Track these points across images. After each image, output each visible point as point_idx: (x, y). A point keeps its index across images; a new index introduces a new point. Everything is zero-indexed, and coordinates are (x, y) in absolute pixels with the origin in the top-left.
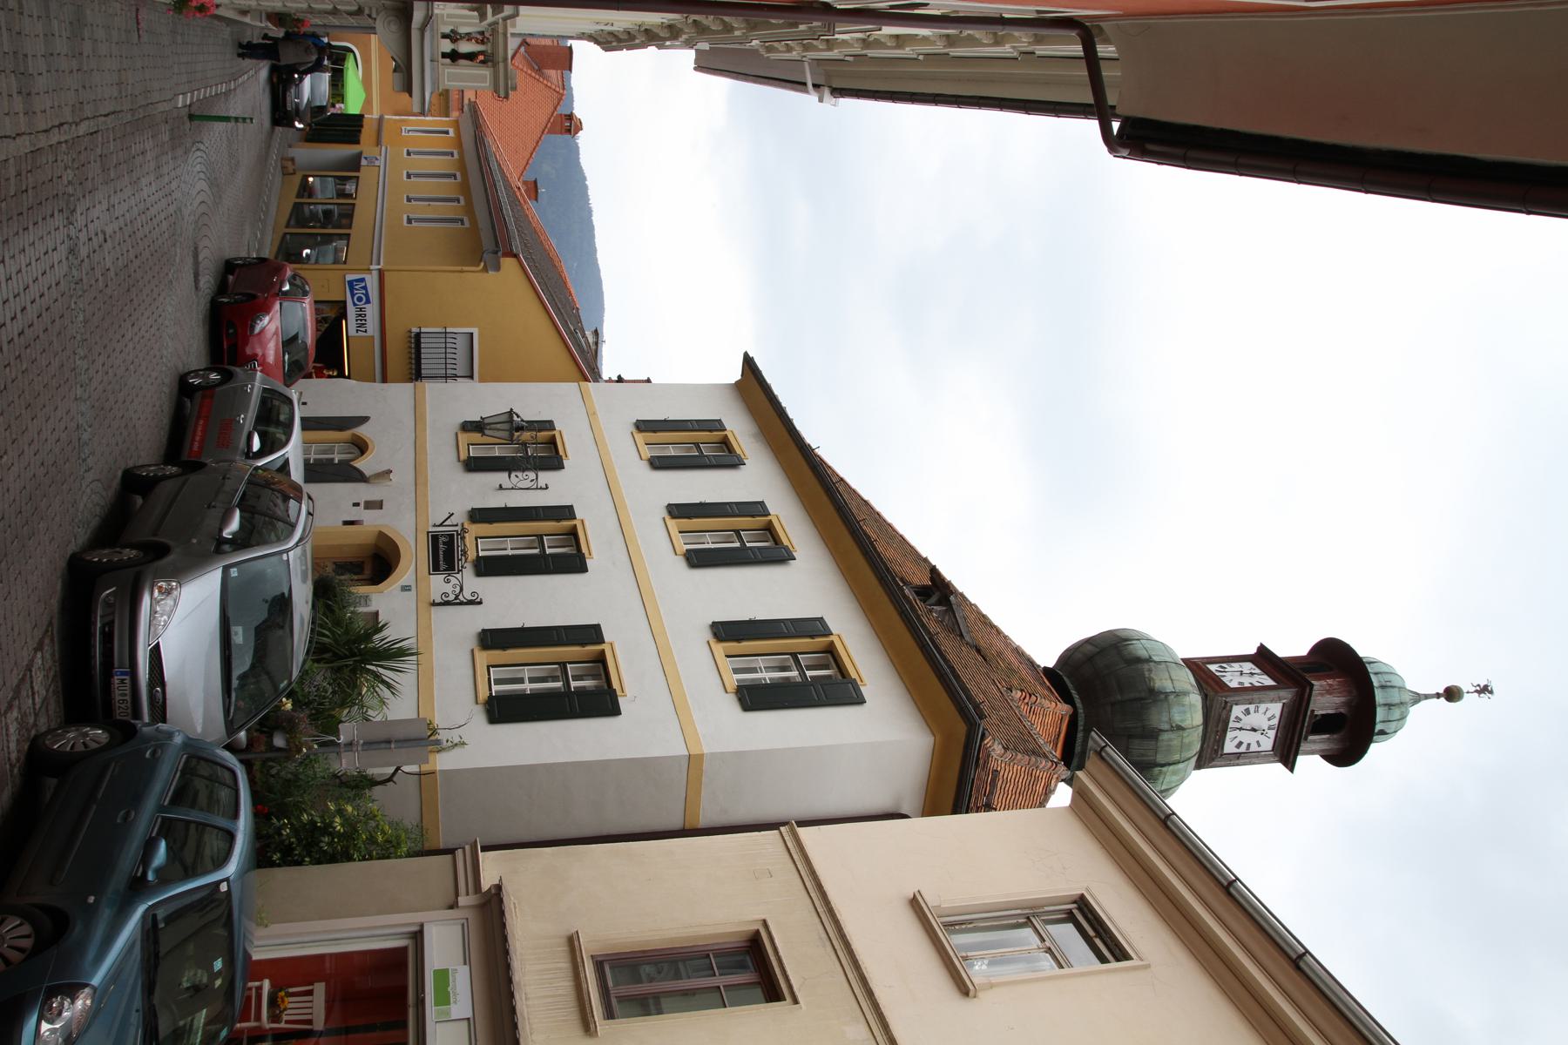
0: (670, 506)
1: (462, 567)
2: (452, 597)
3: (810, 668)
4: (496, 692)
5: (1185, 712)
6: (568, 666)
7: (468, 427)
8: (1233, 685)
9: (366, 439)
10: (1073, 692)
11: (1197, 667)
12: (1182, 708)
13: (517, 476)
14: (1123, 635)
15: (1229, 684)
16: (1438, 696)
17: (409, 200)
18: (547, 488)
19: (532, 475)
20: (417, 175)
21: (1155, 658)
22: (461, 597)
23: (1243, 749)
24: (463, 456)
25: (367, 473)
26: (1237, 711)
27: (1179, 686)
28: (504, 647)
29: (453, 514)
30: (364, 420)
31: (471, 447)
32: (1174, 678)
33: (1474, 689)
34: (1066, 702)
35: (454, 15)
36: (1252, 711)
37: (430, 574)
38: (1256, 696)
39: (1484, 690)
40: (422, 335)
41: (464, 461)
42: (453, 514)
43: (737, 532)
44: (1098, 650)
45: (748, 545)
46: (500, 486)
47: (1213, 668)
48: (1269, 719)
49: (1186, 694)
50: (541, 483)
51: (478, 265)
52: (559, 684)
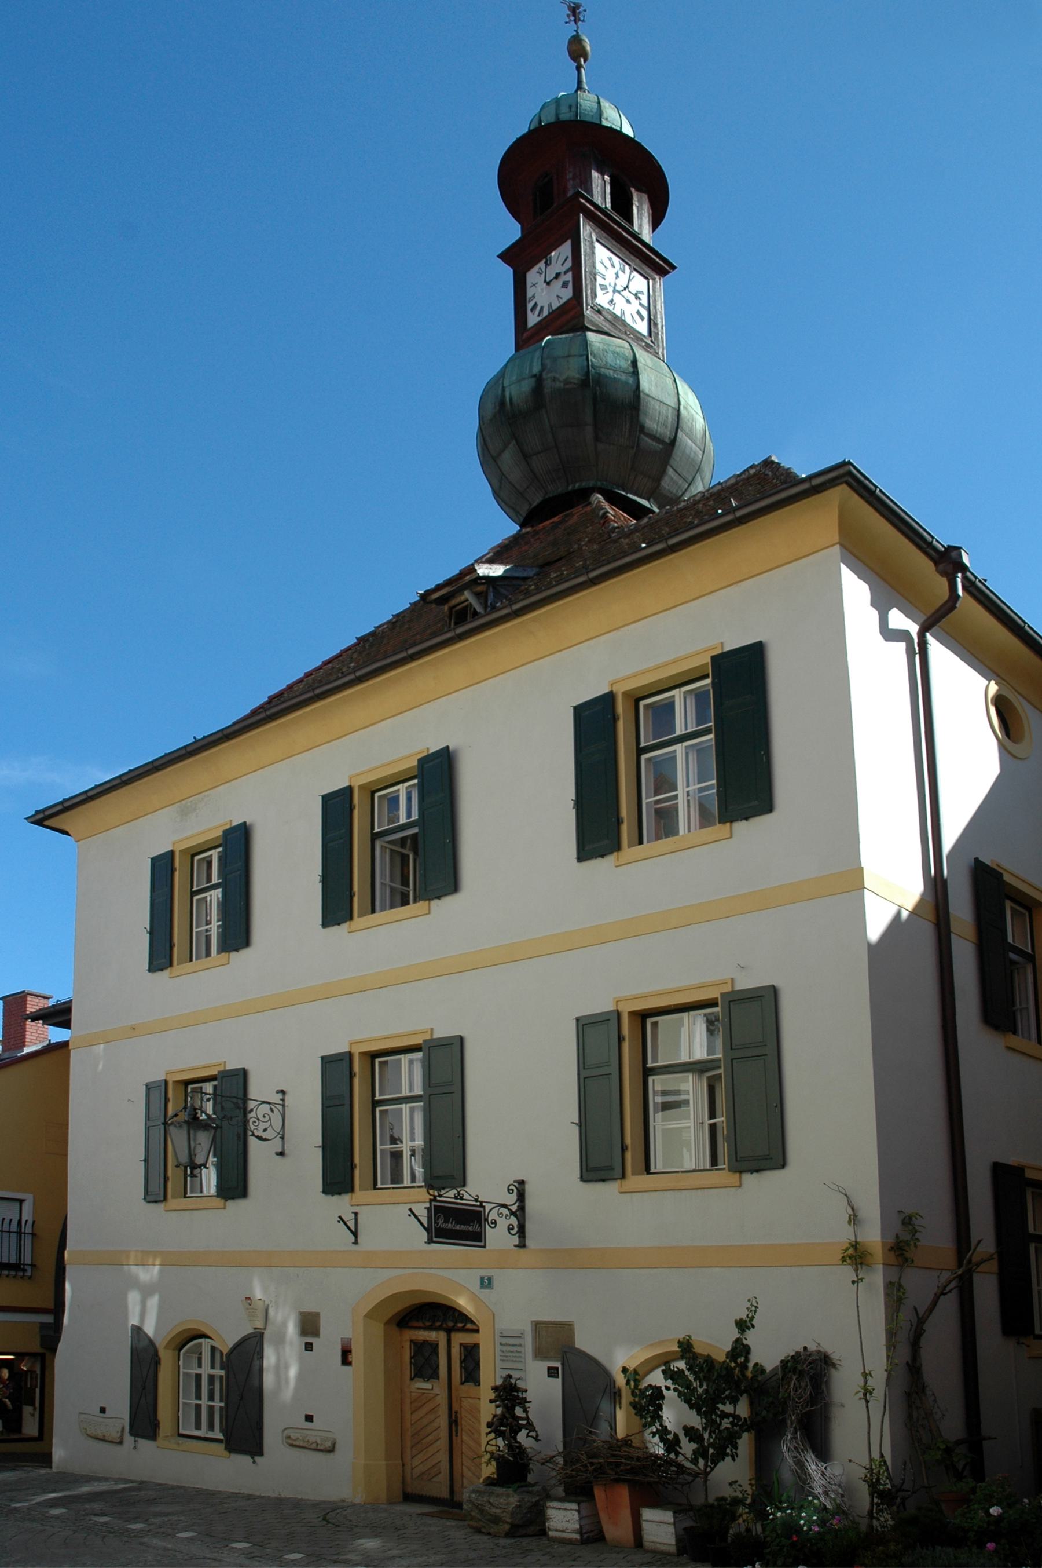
1: (476, 1200)
9: (169, 1338)
13: (265, 1130)
14: (490, 408)
16: (579, 68)
22: (514, 1208)
29: (340, 1217)
32: (566, 354)
35: (315, 702)
37: (484, 1247)
39: (574, 11)
42: (340, 1217)
44: (514, 442)
45: (415, 816)
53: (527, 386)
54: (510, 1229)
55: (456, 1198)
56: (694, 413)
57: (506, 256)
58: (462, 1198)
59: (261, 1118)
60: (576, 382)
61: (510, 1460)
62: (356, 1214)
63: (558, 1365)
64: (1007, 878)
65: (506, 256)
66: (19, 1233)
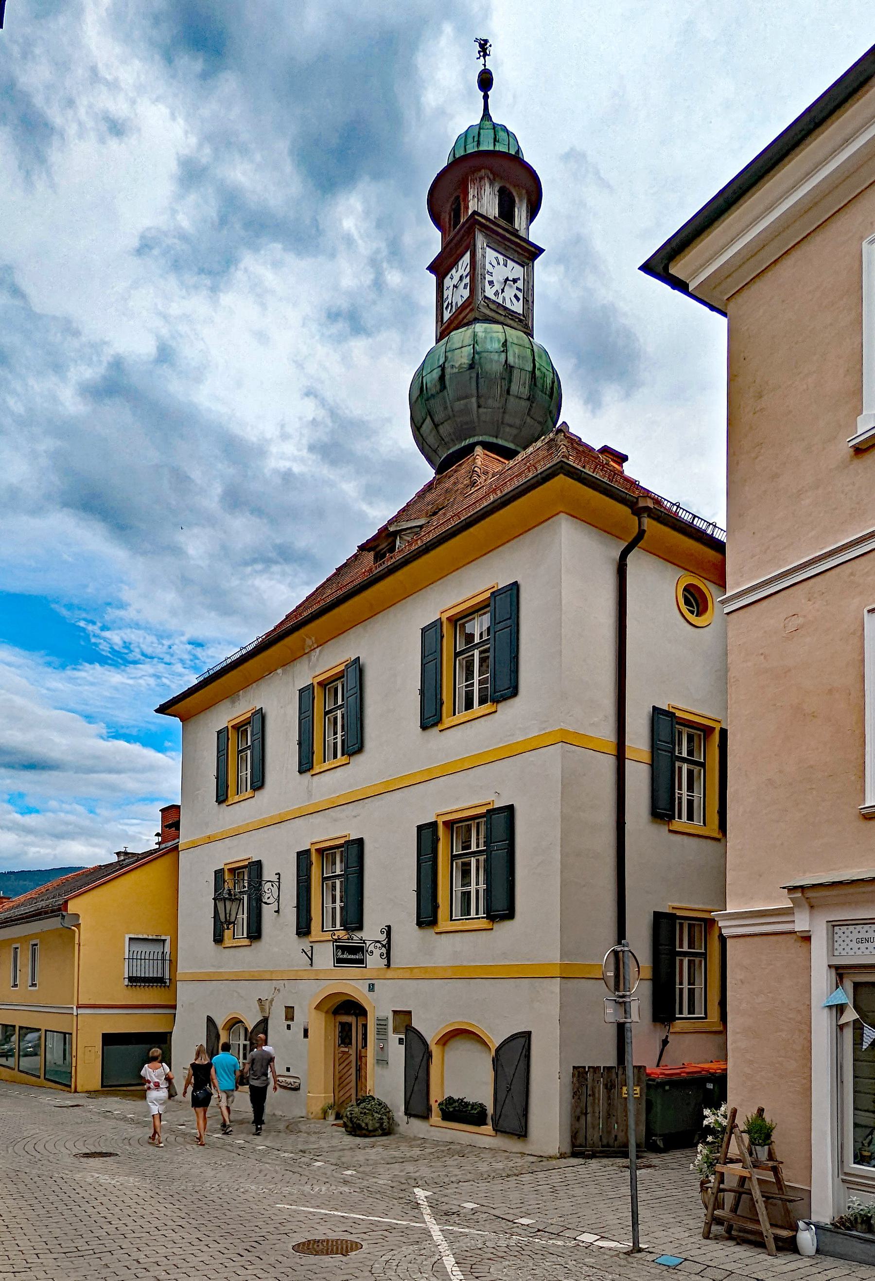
0: (301, 772)
1: (361, 940)
2: (384, 950)
3: (336, 702)
4: (341, 926)
5: (491, 338)
6: (325, 876)
7: (218, 939)
8: (466, 293)
10: (463, 444)
11: (444, 332)
12: (488, 340)
13: (269, 898)
14: (416, 393)
15: (465, 298)
17: (15, 986)
18: (279, 874)
19: (267, 886)
20: (33, 979)
21: (441, 362)
22: (384, 943)
23: (520, 295)
24: (246, 942)
25: (259, 1018)
26: (490, 292)
27: (468, 340)
28: (309, 920)
30: (210, 1020)
31: (454, 918)
32: (461, 346)
33: (482, 58)
34: (473, 451)
36: (491, 279)
37: (366, 967)
38: (479, 271)
40: (131, 975)
41: (251, 942)
43: (240, 752)
45: (249, 744)
46: (275, 912)
47: (447, 315)
48: (499, 264)
49: (475, 335)
50: (275, 878)
51: (74, 931)
52: (338, 882)
53: (436, 374)
54: (381, 955)
55: (348, 939)
56: (546, 371)
57: (432, 268)
58: (352, 940)
59: (267, 891)
60: (465, 366)
61: (693, 1140)
62: (312, 947)
63: (403, 1036)
64: (679, 714)
65: (432, 268)
66: (163, 960)
